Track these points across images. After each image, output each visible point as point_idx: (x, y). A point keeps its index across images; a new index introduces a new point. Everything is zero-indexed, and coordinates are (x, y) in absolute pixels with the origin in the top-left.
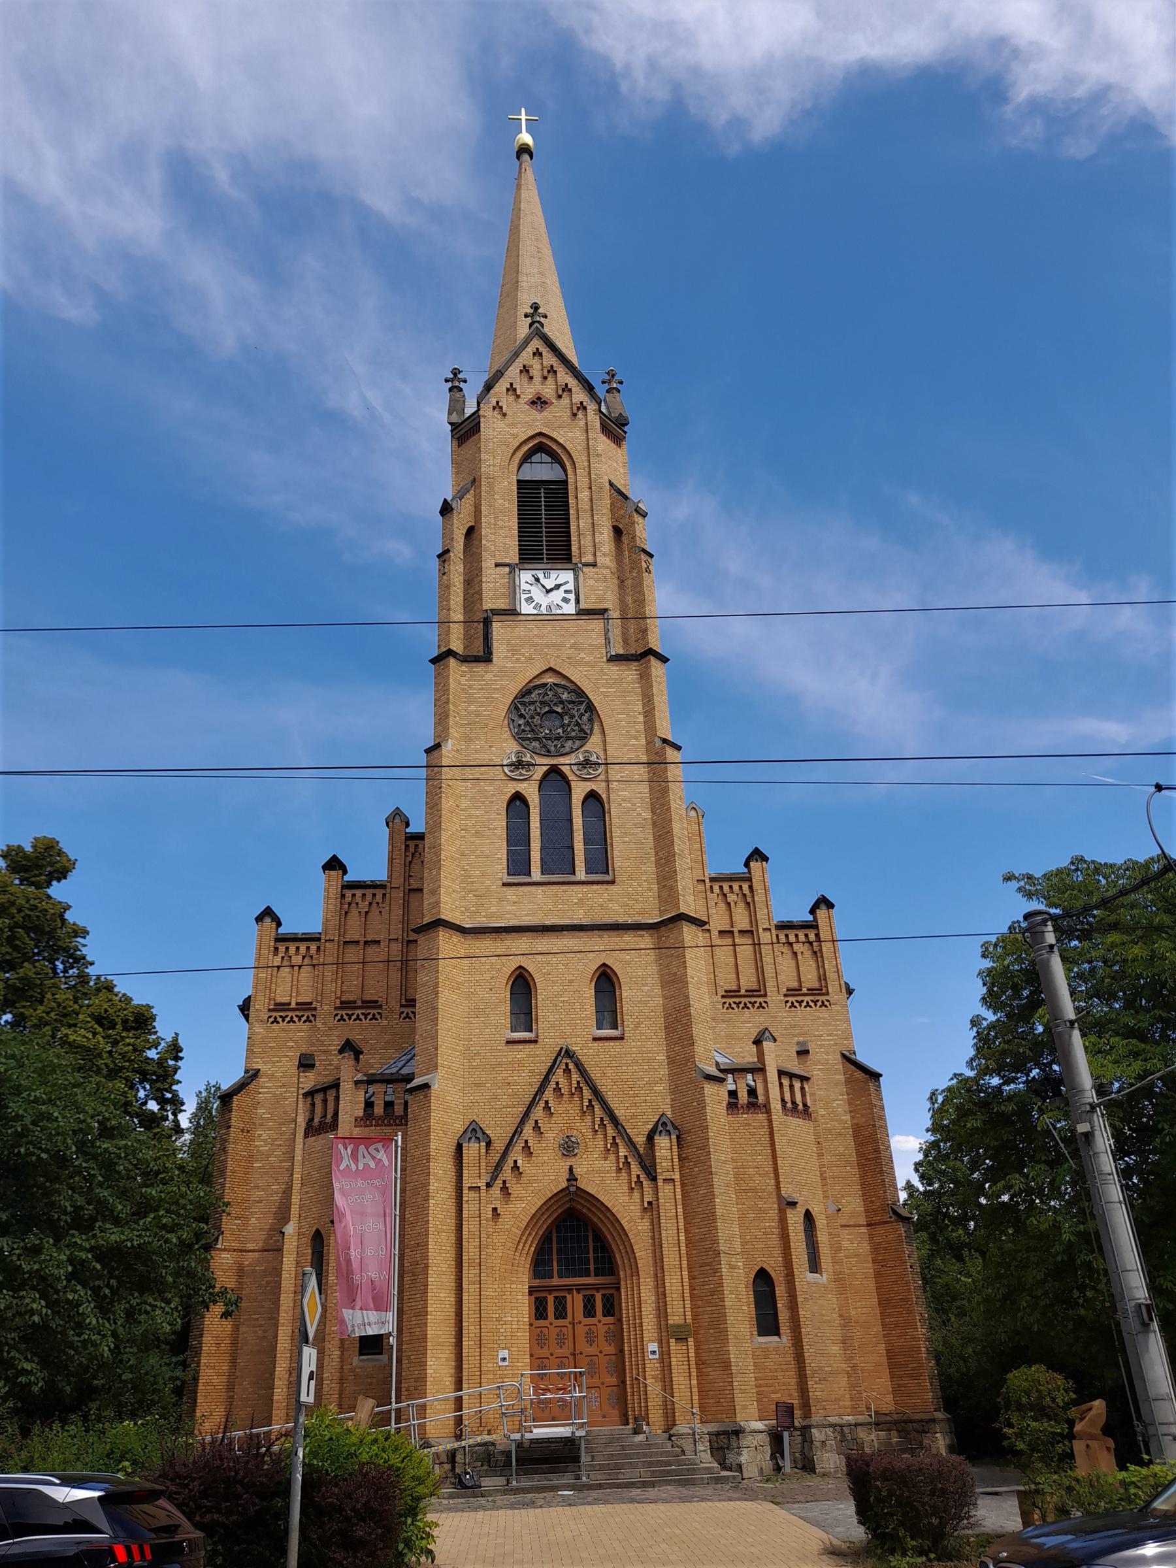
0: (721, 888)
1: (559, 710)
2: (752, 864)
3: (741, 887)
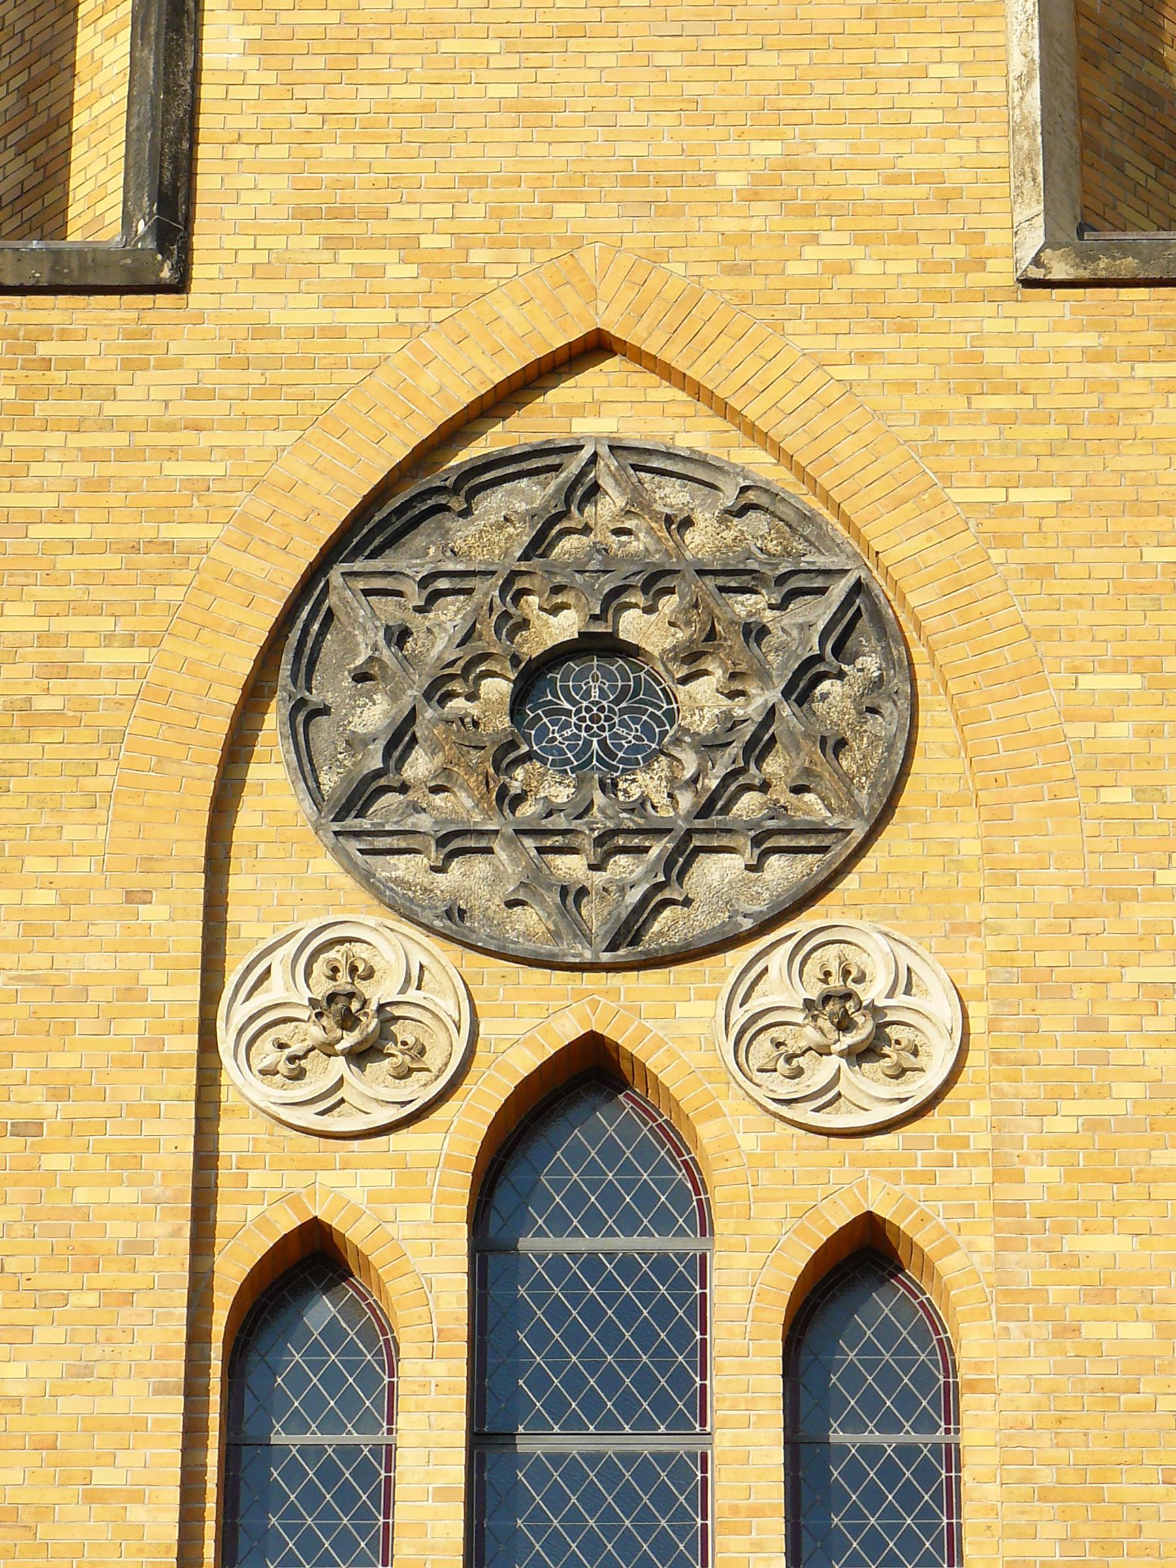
1: (565, 626)
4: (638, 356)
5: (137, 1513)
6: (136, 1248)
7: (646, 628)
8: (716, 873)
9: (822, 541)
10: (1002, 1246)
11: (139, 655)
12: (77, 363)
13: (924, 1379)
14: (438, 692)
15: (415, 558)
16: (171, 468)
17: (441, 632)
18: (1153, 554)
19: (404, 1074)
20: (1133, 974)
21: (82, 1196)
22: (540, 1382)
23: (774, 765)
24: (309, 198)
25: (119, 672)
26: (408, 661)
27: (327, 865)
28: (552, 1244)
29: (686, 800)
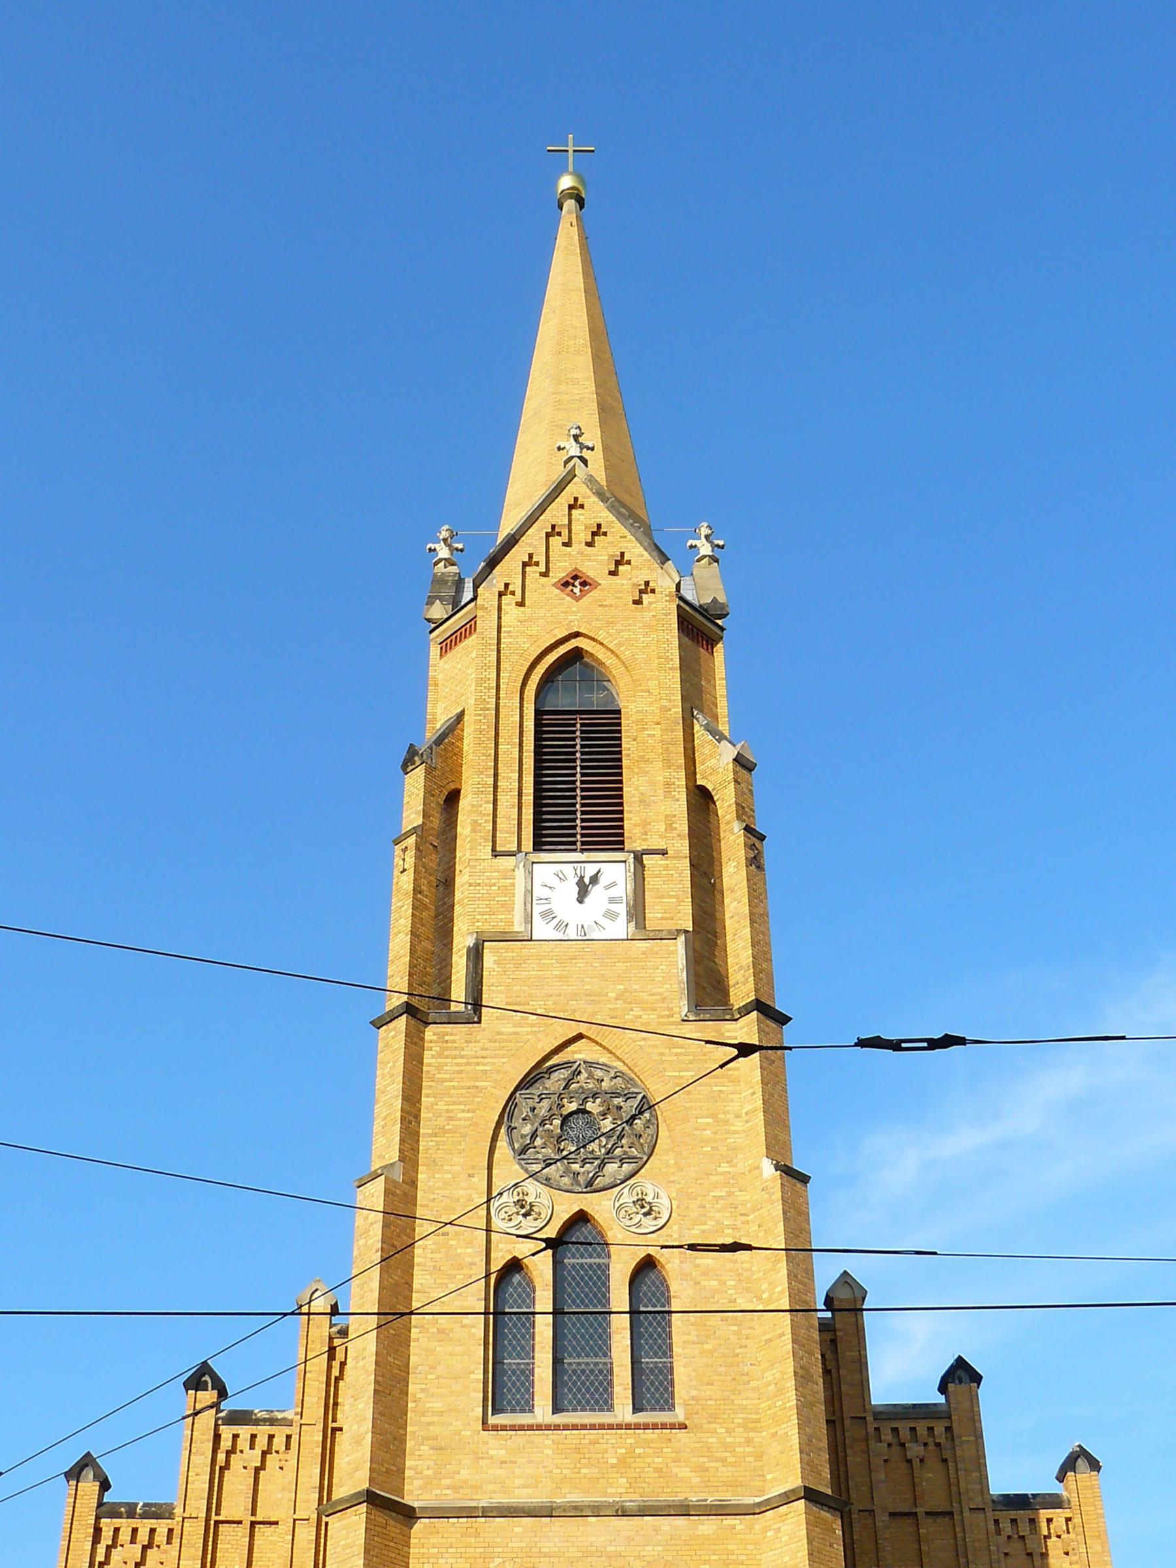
0: (895, 1430)
1: (573, 1107)
4: (590, 1039)
5: (473, 1330)
6: (472, 1264)
7: (593, 1107)
8: (611, 1168)
9: (635, 1085)
10: (681, 1262)
11: (470, 1115)
12: (454, 1041)
13: (663, 1294)
14: (543, 1123)
15: (536, 1090)
16: (478, 1068)
17: (543, 1108)
18: (715, 1088)
19: (536, 1219)
20: (712, 1194)
21: (459, 1251)
22: (569, 1295)
23: (624, 1141)
24: (509, 1000)
25: (466, 1119)
26: (535, 1116)
28: (572, 1261)
29: (603, 1150)
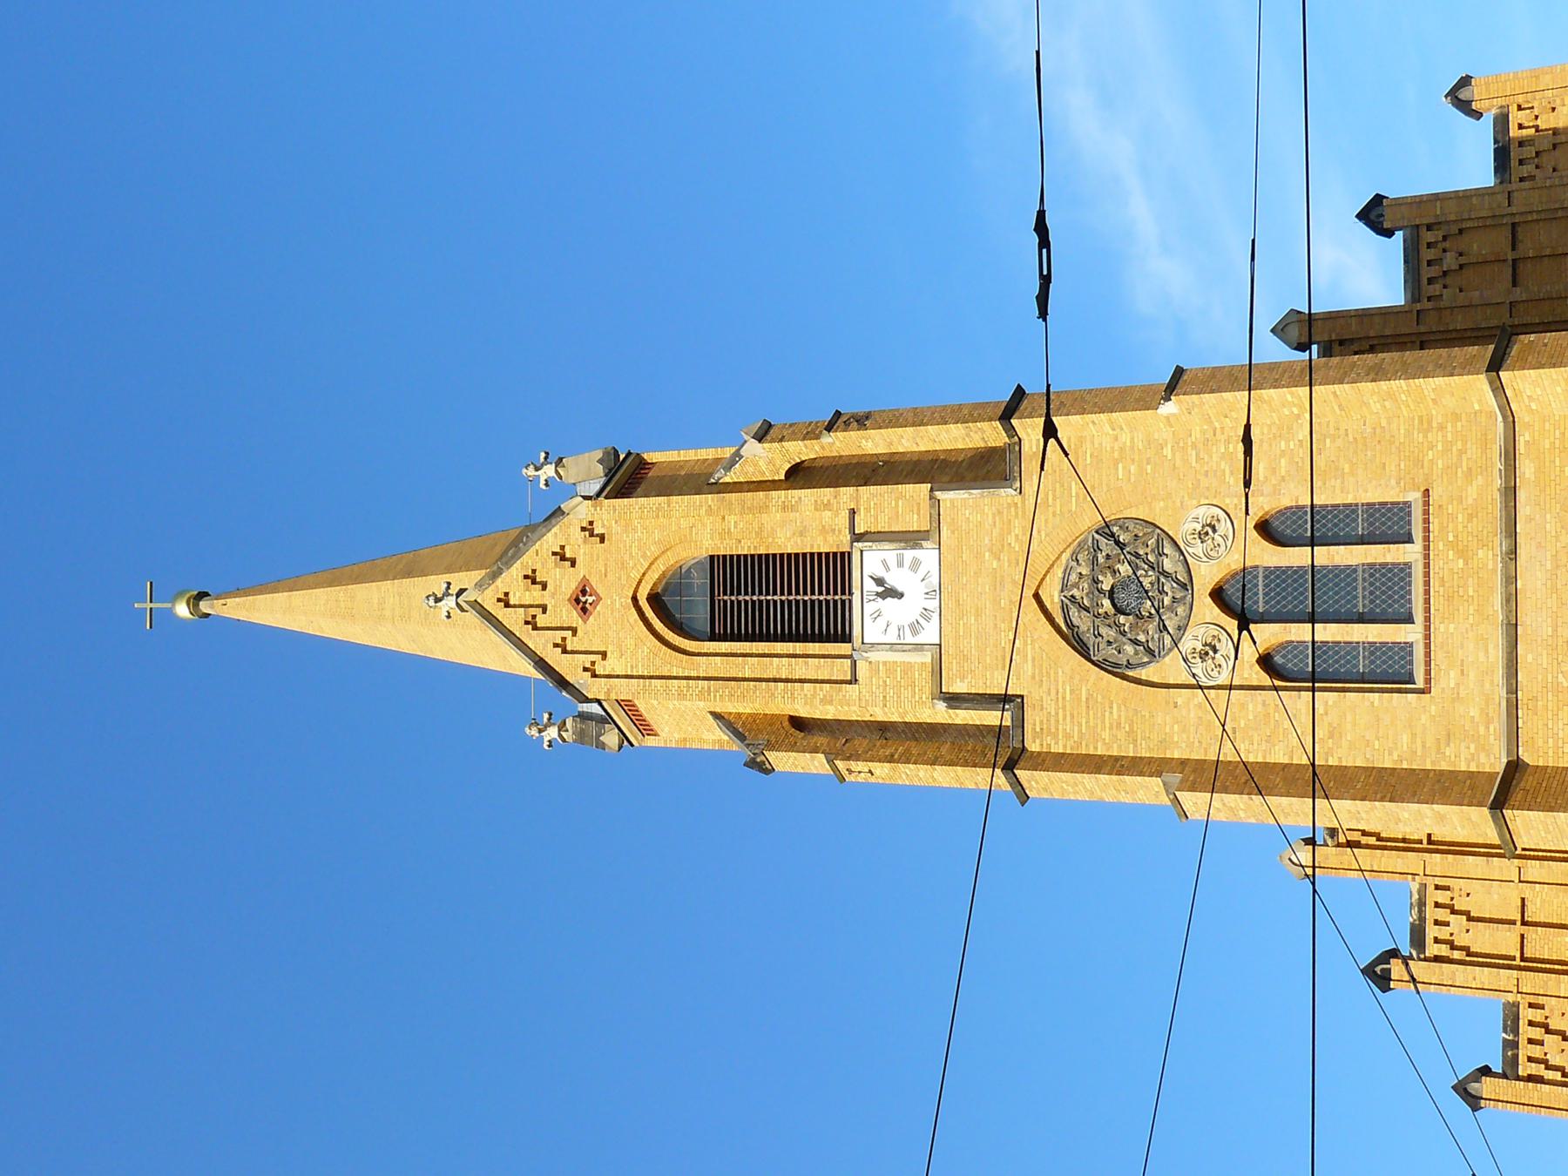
0: (1430, 281)
1: (1106, 602)
2: (1387, 225)
3: (1429, 245)
8: (1168, 565)
14: (1123, 633)
15: (1090, 640)
17: (1108, 633)
27: (1167, 659)
